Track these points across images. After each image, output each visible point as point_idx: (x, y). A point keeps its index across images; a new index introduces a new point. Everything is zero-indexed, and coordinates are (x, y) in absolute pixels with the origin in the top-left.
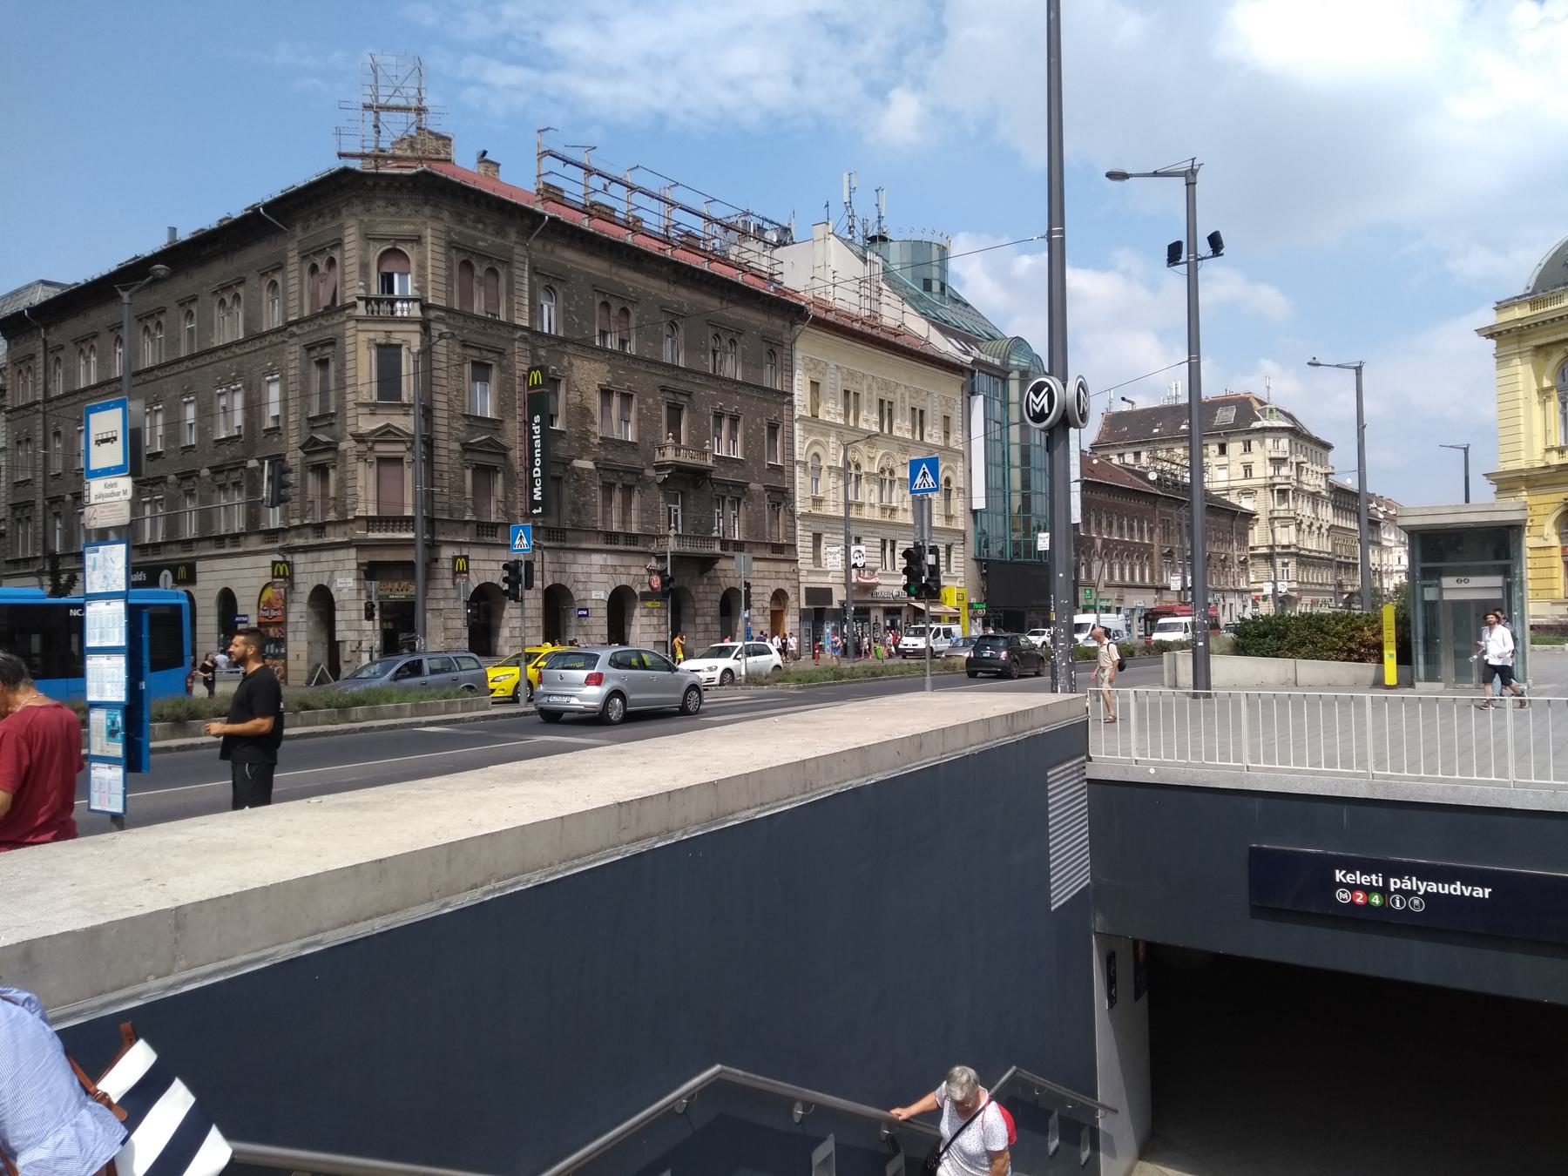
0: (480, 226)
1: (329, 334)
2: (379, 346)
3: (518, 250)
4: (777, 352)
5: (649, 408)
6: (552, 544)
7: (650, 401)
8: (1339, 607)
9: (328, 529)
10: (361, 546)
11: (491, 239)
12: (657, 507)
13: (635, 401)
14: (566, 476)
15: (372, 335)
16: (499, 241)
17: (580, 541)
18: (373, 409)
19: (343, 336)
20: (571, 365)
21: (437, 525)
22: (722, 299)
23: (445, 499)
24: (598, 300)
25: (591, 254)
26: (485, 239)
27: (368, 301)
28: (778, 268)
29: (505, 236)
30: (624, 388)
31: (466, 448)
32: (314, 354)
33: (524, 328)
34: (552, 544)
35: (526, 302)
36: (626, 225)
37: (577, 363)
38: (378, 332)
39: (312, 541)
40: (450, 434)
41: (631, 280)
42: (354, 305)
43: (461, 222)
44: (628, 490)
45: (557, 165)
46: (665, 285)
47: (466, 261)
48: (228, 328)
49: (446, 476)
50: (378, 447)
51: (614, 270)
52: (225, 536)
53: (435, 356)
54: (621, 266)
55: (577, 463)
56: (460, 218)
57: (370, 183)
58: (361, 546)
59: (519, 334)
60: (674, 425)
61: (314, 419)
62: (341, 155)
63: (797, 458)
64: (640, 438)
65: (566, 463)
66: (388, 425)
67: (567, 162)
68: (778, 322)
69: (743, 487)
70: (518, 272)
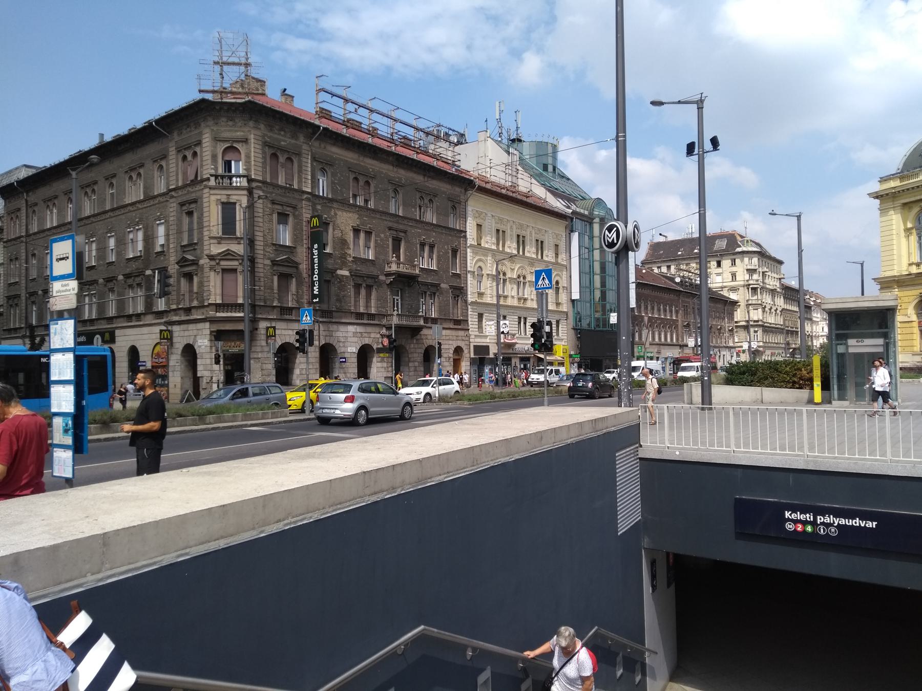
0: (282, 133)
1: (193, 196)
2: (223, 203)
3: (305, 147)
4: (457, 207)
5: (381, 240)
6: (324, 320)
7: (382, 235)
9: (193, 311)
10: (212, 321)
11: (289, 140)
12: (386, 298)
13: (373, 235)
14: (333, 280)
15: (219, 197)
16: (293, 141)
17: (341, 318)
18: (219, 240)
19: (201, 198)
20: (336, 214)
21: (257, 308)
22: (424, 176)
23: (261, 293)
25: (348, 149)
26: (285, 141)
27: (216, 177)
28: (458, 157)
29: (297, 138)
30: (367, 228)
31: (274, 263)
32: (184, 208)
33: (308, 193)
34: (324, 320)
35: (310, 177)
36: (368, 132)
37: (339, 213)
38: (222, 195)
39: (184, 318)
40: (264, 255)
41: (371, 164)
42: (208, 179)
43: (271, 130)
44: (369, 288)
45: (327, 97)
46: (391, 167)
47: (274, 153)
48: (134, 193)
49: (262, 279)
50: (222, 263)
51: (361, 158)
52: (132, 315)
53: (256, 209)
54: (365, 156)
55: (340, 272)
56: (270, 128)
57: (218, 108)
58: (212, 321)
59: (305, 196)
60: (396, 250)
61: (184, 246)
62: (200, 91)
63: (469, 269)
64: (376, 258)
65: (333, 272)
66: (228, 250)
67: (333, 95)
68: (458, 189)
69: (437, 286)
70: (304, 160)
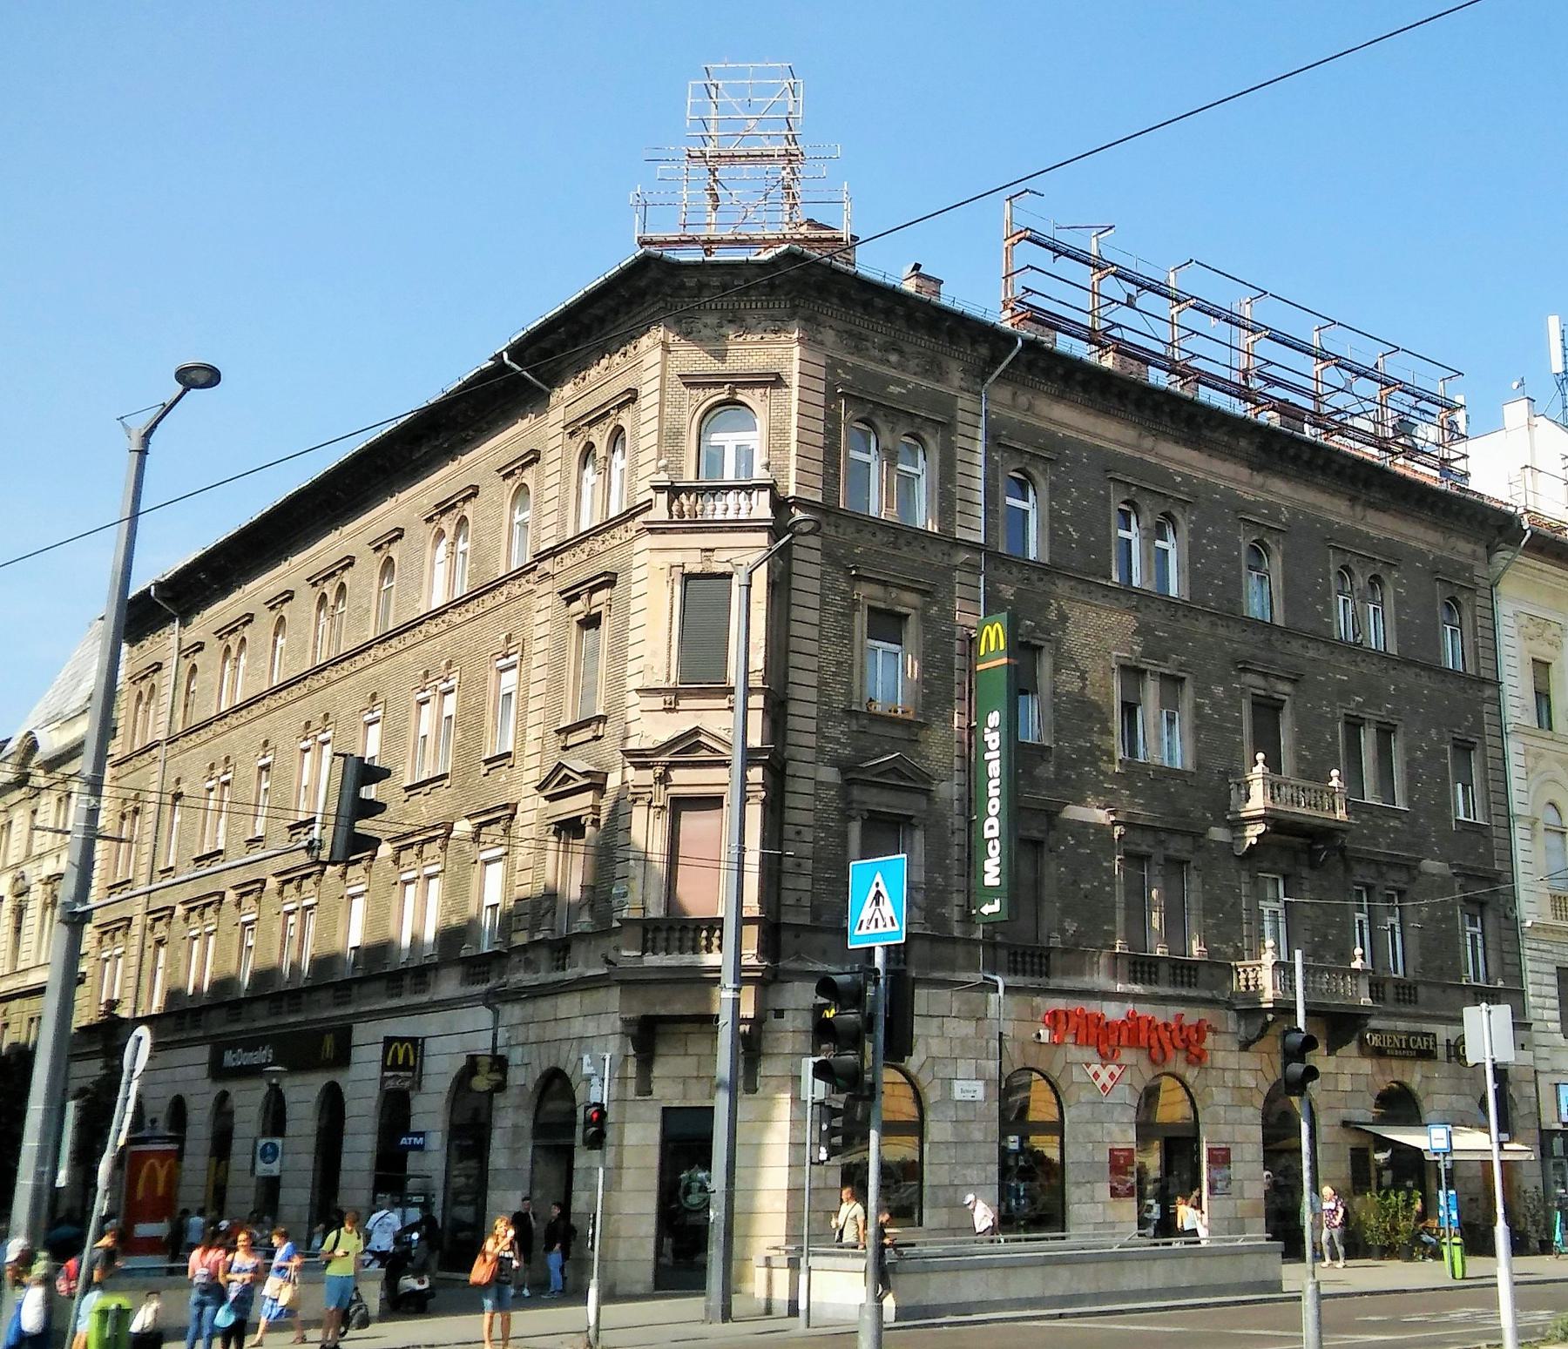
0: (894, 358)
1: (605, 564)
2: (688, 577)
4: (1462, 595)
5: (1215, 705)
7: (1219, 690)
9: (578, 951)
10: (632, 983)
11: (913, 381)
12: (1236, 905)
13: (1188, 690)
14: (1050, 841)
15: (677, 558)
16: (926, 384)
18: (673, 697)
19: (628, 569)
20: (1063, 618)
21: (786, 937)
22: (1353, 500)
23: (805, 883)
24: (1245, 541)
25: (1105, 412)
26: (903, 379)
27: (674, 491)
31: (851, 775)
32: (577, 606)
33: (973, 547)
34: (1138, 989)
35: (980, 498)
38: (688, 551)
39: (544, 976)
40: (820, 750)
41: (1181, 459)
42: (648, 506)
43: (858, 350)
44: (1177, 865)
45: (1043, 257)
46: (1244, 473)
47: (853, 407)
48: (438, 577)
49: (808, 835)
50: (677, 775)
51: (1148, 442)
52: (405, 971)
53: (796, 597)
54: (1160, 434)
55: (1074, 812)
56: (857, 342)
57: (691, 283)
58: (632, 983)
59: (963, 556)
60: (1267, 740)
61: (568, 730)
62: (643, 243)
63: (1516, 808)
64: (1199, 765)
65: (1050, 815)
66: (696, 731)
67: (1058, 251)
68: (1465, 547)
69: (1410, 868)
70: (961, 441)
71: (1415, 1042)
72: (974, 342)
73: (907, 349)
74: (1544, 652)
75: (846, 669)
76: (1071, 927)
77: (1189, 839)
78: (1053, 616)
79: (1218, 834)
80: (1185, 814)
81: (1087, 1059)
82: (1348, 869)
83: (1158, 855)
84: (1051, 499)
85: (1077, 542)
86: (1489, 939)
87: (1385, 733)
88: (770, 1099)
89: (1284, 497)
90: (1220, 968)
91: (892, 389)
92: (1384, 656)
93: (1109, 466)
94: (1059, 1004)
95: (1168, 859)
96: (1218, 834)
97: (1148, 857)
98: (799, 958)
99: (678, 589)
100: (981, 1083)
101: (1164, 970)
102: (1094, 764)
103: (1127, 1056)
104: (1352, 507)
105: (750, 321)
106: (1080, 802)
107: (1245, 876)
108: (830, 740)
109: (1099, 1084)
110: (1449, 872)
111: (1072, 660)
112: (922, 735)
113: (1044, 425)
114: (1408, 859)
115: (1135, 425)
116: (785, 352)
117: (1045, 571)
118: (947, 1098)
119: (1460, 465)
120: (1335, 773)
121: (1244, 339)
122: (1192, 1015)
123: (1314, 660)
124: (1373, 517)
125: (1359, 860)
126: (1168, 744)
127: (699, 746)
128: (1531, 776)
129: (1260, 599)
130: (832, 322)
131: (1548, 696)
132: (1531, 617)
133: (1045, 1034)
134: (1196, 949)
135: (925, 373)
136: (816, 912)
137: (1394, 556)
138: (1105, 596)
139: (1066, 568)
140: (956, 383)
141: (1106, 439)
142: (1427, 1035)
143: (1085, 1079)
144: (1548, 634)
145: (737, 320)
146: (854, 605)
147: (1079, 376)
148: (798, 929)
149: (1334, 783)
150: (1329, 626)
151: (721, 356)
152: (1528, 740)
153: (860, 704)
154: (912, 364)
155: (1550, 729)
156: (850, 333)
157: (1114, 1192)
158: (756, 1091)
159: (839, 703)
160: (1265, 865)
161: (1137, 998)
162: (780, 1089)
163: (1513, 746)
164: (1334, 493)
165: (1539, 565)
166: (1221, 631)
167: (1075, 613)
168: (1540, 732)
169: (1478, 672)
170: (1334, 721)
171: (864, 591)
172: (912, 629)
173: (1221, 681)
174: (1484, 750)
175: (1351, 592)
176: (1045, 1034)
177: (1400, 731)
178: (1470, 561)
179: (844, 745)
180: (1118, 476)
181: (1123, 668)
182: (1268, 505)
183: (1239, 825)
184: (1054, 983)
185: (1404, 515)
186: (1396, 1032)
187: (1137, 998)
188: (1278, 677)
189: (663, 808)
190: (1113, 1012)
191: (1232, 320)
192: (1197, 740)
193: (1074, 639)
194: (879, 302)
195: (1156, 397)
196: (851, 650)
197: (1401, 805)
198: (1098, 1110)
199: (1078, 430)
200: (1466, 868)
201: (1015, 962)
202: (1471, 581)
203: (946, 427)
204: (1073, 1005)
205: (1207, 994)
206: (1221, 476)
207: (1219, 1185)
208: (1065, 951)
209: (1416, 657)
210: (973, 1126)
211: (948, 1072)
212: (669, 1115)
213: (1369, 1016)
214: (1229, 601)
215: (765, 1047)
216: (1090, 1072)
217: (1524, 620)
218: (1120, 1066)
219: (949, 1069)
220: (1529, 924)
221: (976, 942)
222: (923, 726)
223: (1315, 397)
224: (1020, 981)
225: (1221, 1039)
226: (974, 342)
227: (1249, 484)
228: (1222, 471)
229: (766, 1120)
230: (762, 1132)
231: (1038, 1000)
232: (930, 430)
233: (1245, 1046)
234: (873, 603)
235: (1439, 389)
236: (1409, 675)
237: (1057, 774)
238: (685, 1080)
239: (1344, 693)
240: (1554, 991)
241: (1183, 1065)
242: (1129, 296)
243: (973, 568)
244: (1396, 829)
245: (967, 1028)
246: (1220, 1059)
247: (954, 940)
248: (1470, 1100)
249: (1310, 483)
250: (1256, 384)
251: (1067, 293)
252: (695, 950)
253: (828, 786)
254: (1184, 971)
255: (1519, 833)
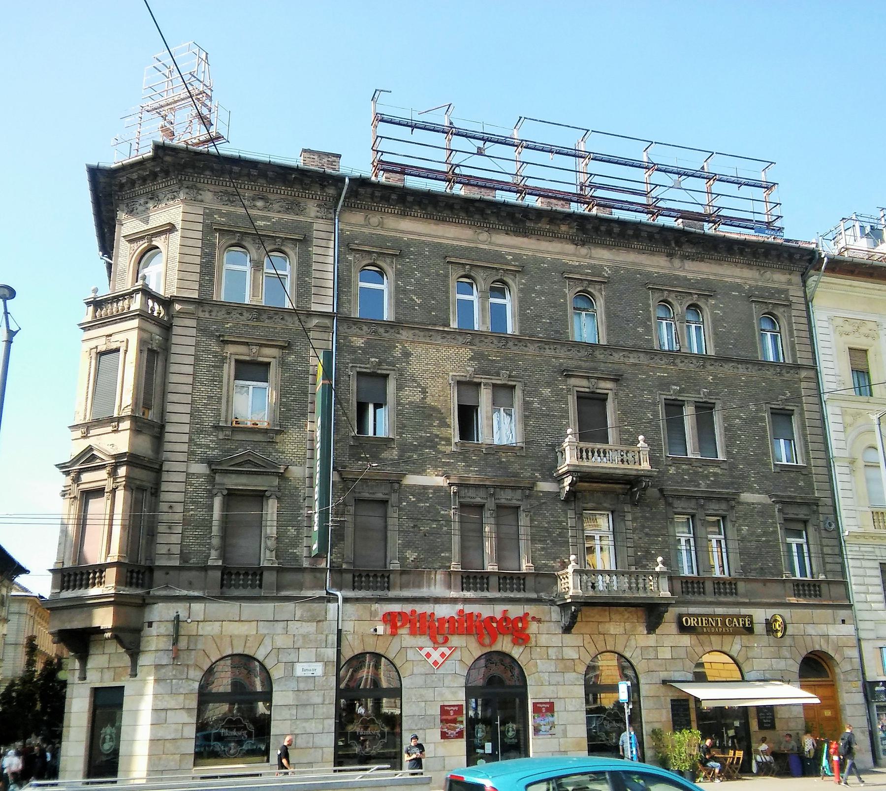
0: (260, 204)
3: (320, 225)
5: (543, 401)
6: (802, 601)
7: (546, 392)
8: (602, 628)
11: (275, 216)
13: (518, 393)
14: (394, 498)
15: (93, 344)
16: (287, 217)
17: (301, 587)
20: (407, 354)
22: (670, 255)
24: (570, 293)
28: (777, 211)
29: (301, 211)
30: (702, 395)
34: (802, 601)
36: (647, 209)
37: (417, 350)
46: (570, 248)
47: (222, 235)
50: (85, 477)
51: (484, 236)
59: (315, 321)
63: (834, 452)
66: (90, 449)
69: (731, 500)
71: (731, 622)
72: (323, 187)
73: (272, 197)
74: (860, 342)
75: (219, 400)
76: (411, 556)
77: (694, 501)
78: (397, 353)
79: (545, 486)
80: (516, 475)
81: (420, 644)
82: (669, 505)
83: (490, 504)
84: (396, 281)
85: (419, 305)
86: (811, 547)
87: (704, 410)
88: (144, 681)
89: (607, 260)
90: (547, 578)
91: (259, 223)
92: (703, 359)
93: (447, 256)
94: (396, 608)
95: (499, 507)
96: (545, 486)
97: (481, 507)
98: (167, 587)
99: (93, 362)
100: (320, 664)
101: (494, 581)
102: (434, 447)
103: (455, 641)
104: (670, 261)
105: (161, 196)
106: (421, 472)
107: (571, 514)
108: (200, 446)
109: (431, 661)
110: (769, 501)
111: (414, 381)
112: (278, 438)
113: (392, 234)
114: (728, 493)
115: (470, 226)
116: (171, 212)
117: (394, 326)
118: (290, 675)
119: (778, 224)
120: (641, 437)
121: (581, 164)
122: (514, 611)
123: (635, 365)
124: (689, 265)
125: (679, 497)
126: (501, 428)
127: (94, 457)
128: (849, 429)
129: (586, 329)
130: (212, 188)
131: (868, 373)
132: (846, 320)
133: (381, 630)
134: (525, 566)
135: (287, 210)
136: (184, 556)
137: (708, 290)
138: (443, 338)
139: (407, 322)
140: (313, 214)
141: (448, 238)
142: (745, 616)
143: (420, 658)
144: (863, 330)
145: (154, 197)
146: (223, 360)
147: (774, 253)
148: (167, 569)
149: (641, 444)
150: (650, 341)
151: (147, 222)
152: (844, 404)
153: (226, 421)
154: (276, 206)
155: (871, 395)
156: (226, 193)
157: (444, 736)
158: (136, 675)
159: (209, 421)
160: (590, 505)
161: (466, 601)
162: (149, 674)
163: (831, 411)
164: (653, 253)
165: (848, 282)
166: (548, 352)
167: (417, 350)
168: (862, 398)
169: (795, 360)
170: (655, 404)
171: (231, 349)
172: (274, 372)
173: (548, 384)
174: (802, 414)
175: (674, 318)
176: (381, 630)
177: (718, 406)
178: (785, 287)
179: (213, 449)
180: (453, 260)
181: (459, 383)
182: (592, 267)
183: (559, 480)
184: (392, 594)
185: (720, 261)
186: (713, 616)
187: (466, 601)
188: (599, 378)
189: (75, 497)
190: (444, 611)
191: (576, 154)
192: (526, 425)
193: (415, 367)
194: (236, 169)
195: (477, 204)
196: (221, 388)
197: (721, 457)
198: (433, 680)
199: (419, 235)
200: (782, 497)
201: (132, 578)
202: (787, 300)
203: (304, 241)
204: (407, 608)
205: (534, 596)
206: (548, 252)
207: (543, 728)
208: (403, 572)
209: (735, 354)
210: (312, 693)
211: (293, 657)
212: (96, 692)
213: (668, 605)
214: (557, 332)
215: (142, 648)
216: (423, 653)
217: (839, 322)
218: (450, 648)
219: (293, 655)
220: (847, 533)
221: (324, 570)
222: (278, 432)
223: (645, 194)
224: (351, 594)
225: (544, 627)
226: (323, 187)
227: (575, 255)
228: (550, 249)
229: (141, 694)
230: (139, 702)
231: (375, 606)
232: (703, 300)
233: (567, 630)
234: (237, 357)
235: (762, 177)
236: (727, 369)
237: (401, 456)
238: (102, 670)
239: (664, 385)
240: (879, 581)
241: (510, 645)
242: (479, 148)
243: (325, 329)
244: (715, 474)
245: (310, 628)
246: (543, 640)
247: (302, 570)
248: (791, 662)
249: (628, 248)
250: (588, 192)
251: (427, 152)
252: (87, 586)
253: (199, 476)
254: (510, 580)
255: (839, 473)
